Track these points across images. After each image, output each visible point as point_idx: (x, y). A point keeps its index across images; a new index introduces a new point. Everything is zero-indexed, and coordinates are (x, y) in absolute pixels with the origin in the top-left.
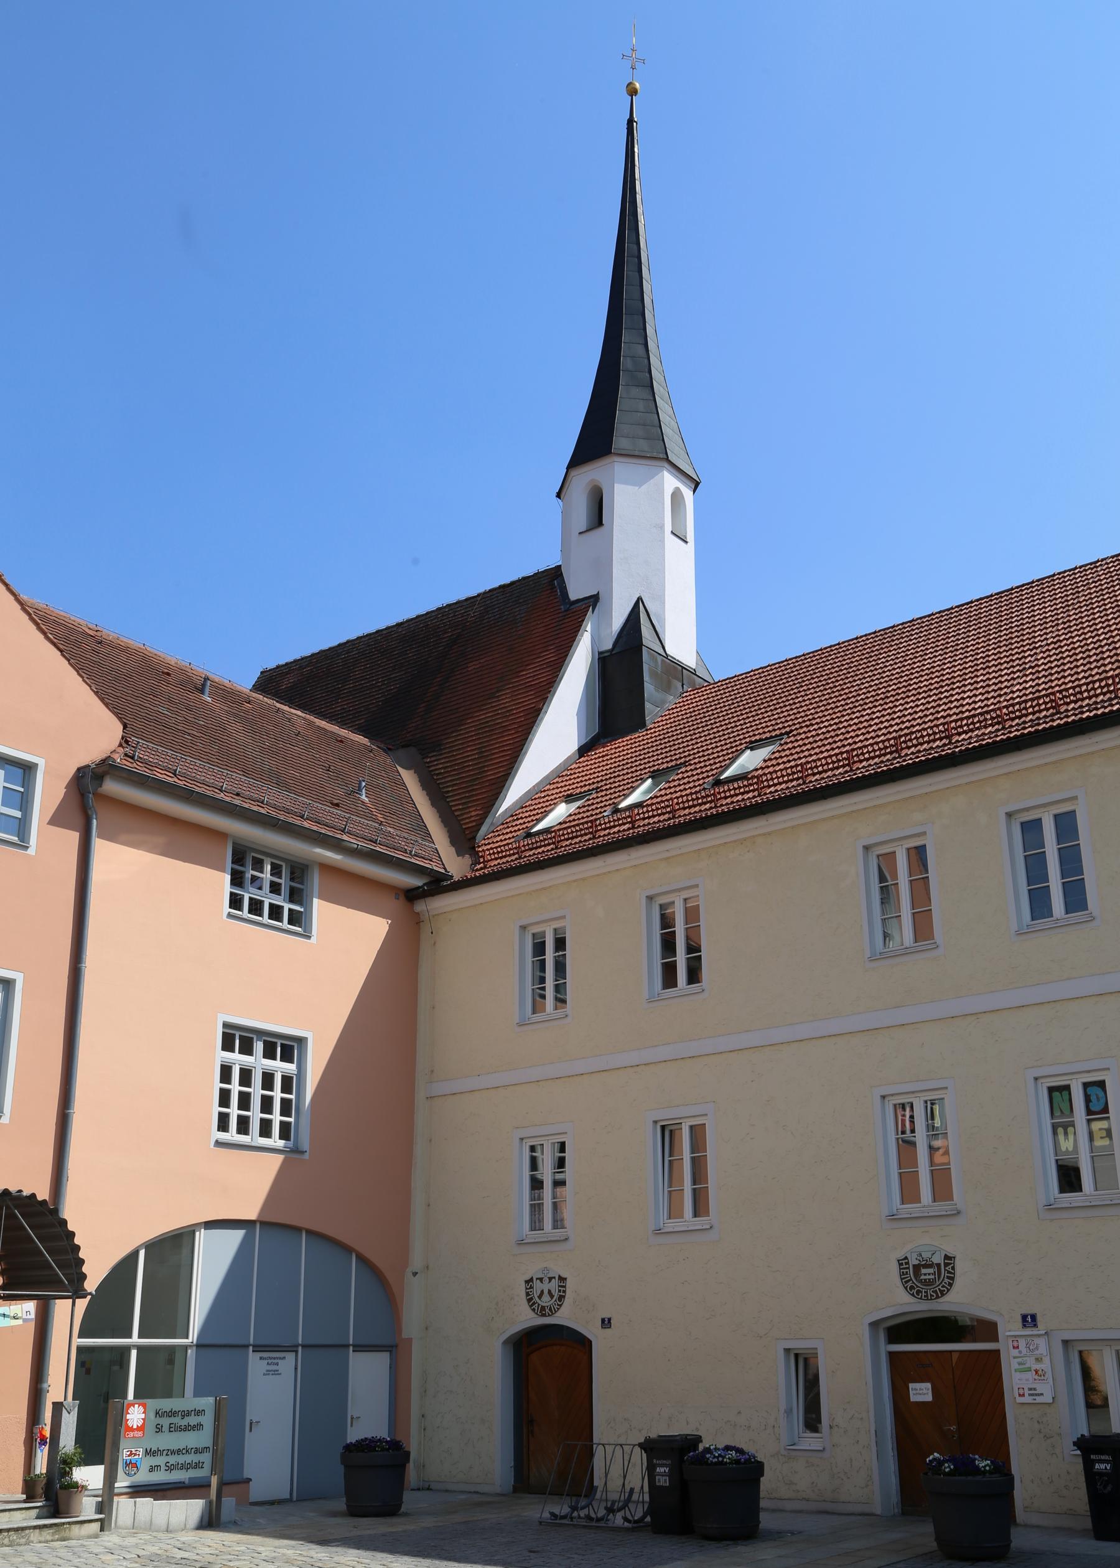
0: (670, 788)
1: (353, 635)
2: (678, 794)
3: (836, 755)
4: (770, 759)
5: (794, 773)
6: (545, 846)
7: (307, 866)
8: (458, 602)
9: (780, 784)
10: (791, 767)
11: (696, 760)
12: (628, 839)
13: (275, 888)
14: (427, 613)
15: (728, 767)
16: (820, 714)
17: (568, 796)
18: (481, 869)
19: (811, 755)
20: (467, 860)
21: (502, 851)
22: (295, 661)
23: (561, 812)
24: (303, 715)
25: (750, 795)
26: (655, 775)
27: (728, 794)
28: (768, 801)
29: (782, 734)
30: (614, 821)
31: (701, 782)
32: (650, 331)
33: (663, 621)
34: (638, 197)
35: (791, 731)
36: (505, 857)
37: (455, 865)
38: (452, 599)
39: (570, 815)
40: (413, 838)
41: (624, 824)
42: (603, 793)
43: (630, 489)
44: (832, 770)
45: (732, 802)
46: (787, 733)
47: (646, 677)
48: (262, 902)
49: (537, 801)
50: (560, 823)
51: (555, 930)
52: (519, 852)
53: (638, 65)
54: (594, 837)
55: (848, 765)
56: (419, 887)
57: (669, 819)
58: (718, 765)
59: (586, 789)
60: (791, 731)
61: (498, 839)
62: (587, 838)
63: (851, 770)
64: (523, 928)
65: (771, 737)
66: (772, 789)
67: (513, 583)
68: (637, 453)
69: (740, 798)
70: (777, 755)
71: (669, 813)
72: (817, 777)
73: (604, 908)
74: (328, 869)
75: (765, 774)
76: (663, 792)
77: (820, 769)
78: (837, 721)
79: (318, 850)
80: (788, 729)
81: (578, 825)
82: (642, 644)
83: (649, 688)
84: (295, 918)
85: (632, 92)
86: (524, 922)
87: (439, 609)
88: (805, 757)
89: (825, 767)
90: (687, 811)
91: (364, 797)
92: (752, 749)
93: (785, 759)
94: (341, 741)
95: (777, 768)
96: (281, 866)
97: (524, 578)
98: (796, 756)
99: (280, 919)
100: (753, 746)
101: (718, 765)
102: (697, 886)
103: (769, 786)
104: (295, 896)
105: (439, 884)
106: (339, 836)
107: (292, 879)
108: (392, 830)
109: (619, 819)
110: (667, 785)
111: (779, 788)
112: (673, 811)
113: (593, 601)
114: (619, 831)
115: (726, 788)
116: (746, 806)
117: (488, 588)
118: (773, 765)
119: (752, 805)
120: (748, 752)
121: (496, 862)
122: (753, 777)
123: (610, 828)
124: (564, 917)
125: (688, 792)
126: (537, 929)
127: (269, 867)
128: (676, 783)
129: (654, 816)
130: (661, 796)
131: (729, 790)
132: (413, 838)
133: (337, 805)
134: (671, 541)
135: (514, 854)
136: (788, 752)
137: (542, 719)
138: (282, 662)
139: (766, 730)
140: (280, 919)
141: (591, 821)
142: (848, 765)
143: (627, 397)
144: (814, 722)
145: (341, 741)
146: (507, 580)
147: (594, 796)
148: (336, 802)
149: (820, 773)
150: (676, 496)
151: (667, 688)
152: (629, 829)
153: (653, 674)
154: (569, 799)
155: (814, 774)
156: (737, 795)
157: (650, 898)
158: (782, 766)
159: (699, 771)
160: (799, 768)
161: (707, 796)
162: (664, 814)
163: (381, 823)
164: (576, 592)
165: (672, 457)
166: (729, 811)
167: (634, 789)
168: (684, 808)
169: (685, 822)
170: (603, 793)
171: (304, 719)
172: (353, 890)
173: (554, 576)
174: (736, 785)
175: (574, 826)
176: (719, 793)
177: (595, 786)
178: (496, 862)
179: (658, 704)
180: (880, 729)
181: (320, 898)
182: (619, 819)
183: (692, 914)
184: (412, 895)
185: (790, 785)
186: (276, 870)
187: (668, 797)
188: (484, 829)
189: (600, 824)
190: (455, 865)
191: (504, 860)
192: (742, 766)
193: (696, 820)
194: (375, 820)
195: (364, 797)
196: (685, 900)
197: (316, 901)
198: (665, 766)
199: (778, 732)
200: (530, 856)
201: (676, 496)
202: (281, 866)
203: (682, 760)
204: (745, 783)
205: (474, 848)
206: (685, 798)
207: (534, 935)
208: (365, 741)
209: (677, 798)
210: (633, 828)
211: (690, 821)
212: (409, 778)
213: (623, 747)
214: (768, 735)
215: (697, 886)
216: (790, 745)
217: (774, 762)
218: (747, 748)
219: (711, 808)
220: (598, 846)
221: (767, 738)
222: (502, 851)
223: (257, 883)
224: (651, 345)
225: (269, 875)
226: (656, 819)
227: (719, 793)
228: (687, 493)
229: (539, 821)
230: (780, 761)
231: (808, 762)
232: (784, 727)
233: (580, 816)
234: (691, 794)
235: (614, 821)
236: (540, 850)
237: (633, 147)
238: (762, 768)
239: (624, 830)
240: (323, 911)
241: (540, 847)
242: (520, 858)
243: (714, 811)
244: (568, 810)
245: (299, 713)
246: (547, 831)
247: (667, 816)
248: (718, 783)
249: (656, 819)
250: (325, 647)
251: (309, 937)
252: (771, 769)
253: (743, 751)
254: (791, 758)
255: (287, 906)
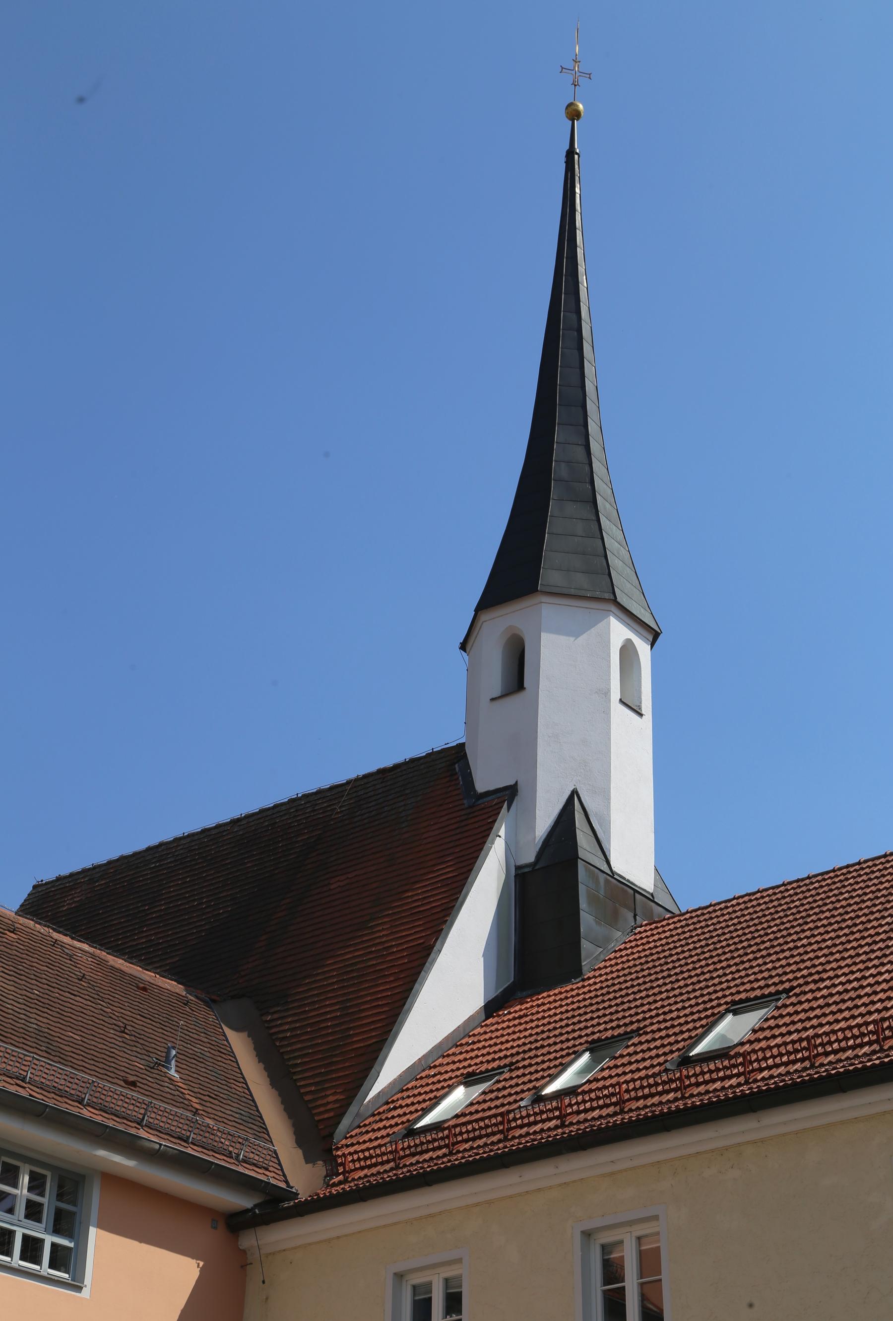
0: (616, 1067)
1: (167, 835)
2: (629, 1077)
3: (859, 1026)
4: (762, 1029)
5: (796, 1051)
6: (434, 1149)
7: (83, 1177)
8: (320, 792)
9: (777, 1066)
10: (793, 1042)
11: (655, 1027)
12: (555, 1142)
13: (33, 1212)
14: (276, 806)
15: (700, 1038)
16: (834, 965)
17: (469, 1075)
18: (340, 1183)
19: (821, 1025)
20: (320, 1169)
21: (371, 1157)
22: (84, 871)
23: (458, 1097)
24: (91, 950)
25: (734, 1081)
26: (596, 1047)
27: (701, 1079)
28: (760, 1091)
29: (778, 993)
30: (535, 1114)
31: (662, 1059)
32: (592, 427)
33: (606, 822)
34: (580, 252)
35: (792, 988)
36: (375, 1165)
37: (301, 1176)
38: (311, 786)
39: (472, 1104)
40: (242, 1134)
41: (549, 1119)
42: (520, 1072)
43: (563, 640)
44: (853, 1048)
45: (707, 1092)
46: (787, 991)
47: (583, 904)
48: (12, 1233)
49: (423, 1082)
50: (457, 1116)
51: (447, 1280)
52: (396, 1158)
53: (582, 81)
54: (506, 1139)
55: (877, 1041)
56: (247, 1211)
57: (615, 1114)
58: (686, 1035)
59: (495, 1064)
60: (792, 988)
61: (366, 1137)
62: (495, 1139)
63: (882, 1050)
64: (399, 1277)
65: (763, 996)
66: (765, 1074)
67: (396, 767)
68: (573, 592)
69: (718, 1085)
70: (772, 1023)
71: (615, 1104)
72: (831, 1058)
73: (516, 1247)
74: (114, 1181)
75: (754, 1051)
76: (606, 1073)
77: (836, 1046)
78: (858, 975)
79: (102, 1153)
80: (787, 985)
81: (482, 1119)
82: (577, 857)
83: (587, 919)
84: (60, 1258)
85: (574, 115)
86: (400, 1267)
87: (292, 801)
88: (813, 1027)
89: (843, 1044)
90: (641, 1103)
91: (172, 1072)
92: (735, 1013)
93: (784, 1030)
94: (145, 989)
95: (773, 1043)
96: (45, 1177)
97: (413, 761)
98: (799, 1026)
99: (37, 1260)
100: (737, 1008)
101: (686, 1035)
102: (656, 1218)
103: (761, 1070)
104: (64, 1223)
105: (277, 1206)
106: (133, 1131)
107: (60, 1196)
108: (211, 1122)
109: (542, 1112)
110: (612, 1063)
111: (775, 1072)
112: (621, 1102)
113: (509, 794)
114: (542, 1130)
115: (698, 1069)
116: (727, 1099)
117: (362, 773)
118: (766, 1039)
119: (735, 1097)
120: (729, 1017)
121: (362, 1174)
122: (738, 1055)
123: (529, 1125)
124: (459, 1261)
125: (643, 1073)
126: (418, 1279)
127: (27, 1179)
128: (625, 1060)
129: (593, 1109)
130: (604, 1078)
131: (703, 1073)
132: (242, 1134)
133: (133, 1084)
134: (619, 713)
135: (388, 1162)
136: (787, 1020)
137: (434, 960)
138: (65, 872)
139: (756, 985)
140: (37, 1260)
141: (502, 1114)
142: (877, 1041)
143: (560, 515)
144: (825, 976)
145: (145, 989)
146: (388, 763)
147: (507, 1076)
148: (132, 1079)
149: (836, 1052)
150: (628, 651)
151: (611, 919)
152: (556, 1127)
153: (593, 899)
154: (469, 1080)
155: (827, 1054)
156: (713, 1081)
157: (587, 1235)
158: (779, 1040)
159: (658, 1043)
160: (805, 1044)
161: (671, 1081)
162: (607, 1106)
163: (196, 1112)
164: (486, 779)
165: (621, 598)
166: (702, 1105)
167: (564, 1067)
168: (637, 1099)
169: (638, 1120)
170: (520, 1072)
171: (93, 955)
172: (151, 1215)
173: (456, 757)
174: (712, 1067)
175: (477, 1121)
176: (688, 1077)
177: (507, 1061)
178: (362, 1174)
179: (601, 944)
180: (858, 955)
181: (100, 1226)
182: (542, 1112)
183: (649, 1261)
184: (236, 1223)
185: (792, 1068)
186: (37, 1184)
187: (614, 1081)
188: (346, 1122)
189: (515, 1119)
190: (301, 1176)
191: (374, 1170)
192: (722, 1037)
193: (654, 1116)
194: (187, 1107)
195: (172, 1072)
196: (639, 1239)
197: (93, 1231)
198: (609, 1034)
199: (772, 989)
200: (412, 1164)
201: (628, 651)
202: (45, 1177)
203: (635, 1026)
204: (726, 1063)
205: (330, 1151)
206: (638, 1083)
207: (414, 1287)
208: (179, 989)
209: (627, 1082)
210: (563, 1125)
211: (646, 1117)
212: (239, 1044)
213: (550, 1002)
214: (758, 993)
215: (656, 1218)
216: (790, 1009)
217: (768, 1033)
218: (728, 1011)
219: (676, 1099)
220: (511, 1152)
221: (756, 998)
222: (371, 1157)
223: (6, 1203)
224: (594, 446)
225: (25, 1191)
226: (596, 1113)
227: (688, 1077)
228: (643, 648)
229: (426, 1111)
230: (777, 1032)
231: (817, 1036)
232: (782, 982)
233: (485, 1106)
234: (647, 1077)
235: (535, 1114)
236: (426, 1156)
237: (573, 187)
238: (750, 1042)
239: (548, 1128)
240: (100, 1245)
241: (427, 1151)
242: (397, 1167)
243: (680, 1104)
244: (467, 1095)
245: (86, 947)
246: (436, 1127)
247: (611, 1110)
248: (686, 1061)
249: (596, 1113)
250: (128, 851)
251: (79, 1289)
252: (763, 1044)
253: (722, 1016)
254: (792, 1028)
255: (49, 1240)
